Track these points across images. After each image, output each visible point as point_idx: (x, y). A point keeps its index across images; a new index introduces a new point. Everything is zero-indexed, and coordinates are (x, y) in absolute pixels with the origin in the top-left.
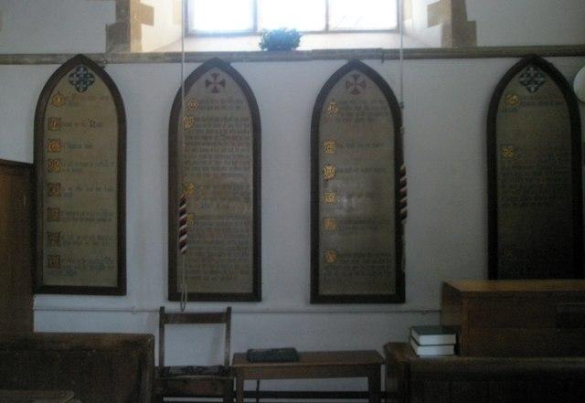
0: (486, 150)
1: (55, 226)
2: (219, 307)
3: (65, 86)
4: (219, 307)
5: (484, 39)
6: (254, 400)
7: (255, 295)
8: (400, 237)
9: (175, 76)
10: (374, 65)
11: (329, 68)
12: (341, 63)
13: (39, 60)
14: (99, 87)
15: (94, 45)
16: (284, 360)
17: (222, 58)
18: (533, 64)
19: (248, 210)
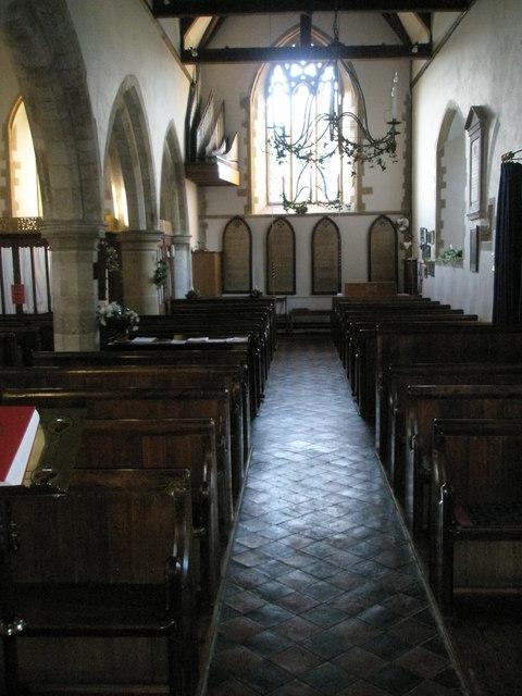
0: (145, 129)
1: (229, 272)
2: (283, 296)
3: (232, 226)
4: (283, 296)
5: (368, 209)
6: (28, 203)
7: (294, 292)
8: (147, 172)
9: (265, 223)
10: (332, 218)
11: (317, 219)
12: (321, 218)
13: (223, 217)
14: (243, 227)
15: (240, 212)
16: (304, 312)
17: (90, 124)
18: (383, 217)
19: (291, 264)
